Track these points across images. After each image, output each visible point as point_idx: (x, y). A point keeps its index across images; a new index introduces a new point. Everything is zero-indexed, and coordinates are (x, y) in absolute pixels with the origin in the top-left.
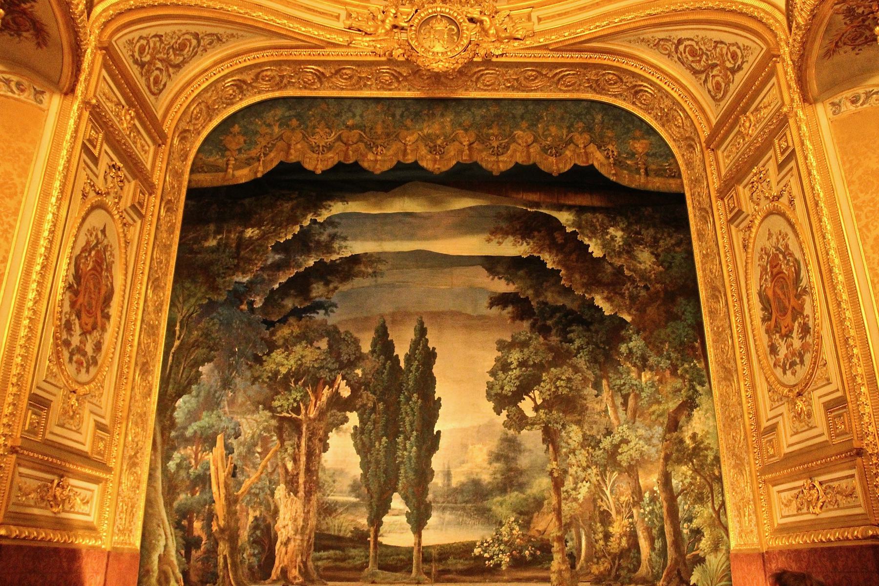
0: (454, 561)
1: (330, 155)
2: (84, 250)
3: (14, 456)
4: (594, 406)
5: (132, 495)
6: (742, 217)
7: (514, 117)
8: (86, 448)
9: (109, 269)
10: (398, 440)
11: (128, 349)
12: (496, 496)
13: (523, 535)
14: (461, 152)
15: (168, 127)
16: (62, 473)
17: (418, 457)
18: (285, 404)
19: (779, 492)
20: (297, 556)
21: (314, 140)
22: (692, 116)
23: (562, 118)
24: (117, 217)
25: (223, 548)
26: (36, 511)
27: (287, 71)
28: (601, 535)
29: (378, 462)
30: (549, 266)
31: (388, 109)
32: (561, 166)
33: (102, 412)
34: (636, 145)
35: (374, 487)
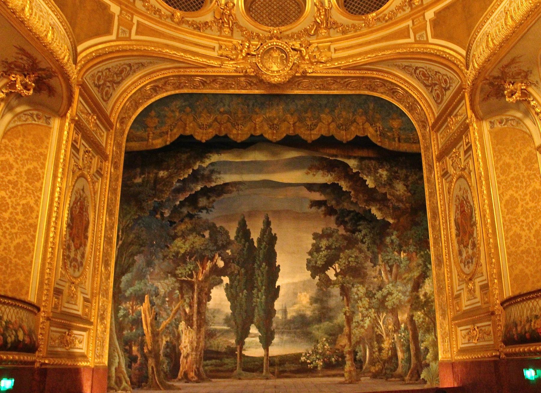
0: (289, 365)
1: (210, 130)
2: (74, 204)
3: (49, 322)
4: (371, 272)
5: (102, 336)
6: (448, 175)
7: (321, 106)
8: (80, 313)
9: (87, 211)
10: (254, 292)
11: (98, 254)
12: (315, 324)
13: (331, 349)
14: (289, 128)
15: (114, 119)
16: (70, 328)
17: (266, 302)
18: (184, 272)
19: (461, 330)
20: (193, 365)
21: (201, 121)
22: (425, 110)
23: (350, 107)
24: (89, 180)
25: (151, 362)
26: (59, 349)
27: (183, 80)
28: (377, 349)
29: (241, 305)
30: (344, 189)
31: (245, 101)
32: (348, 137)
33: (86, 292)
34: (393, 123)
35: (239, 321)
